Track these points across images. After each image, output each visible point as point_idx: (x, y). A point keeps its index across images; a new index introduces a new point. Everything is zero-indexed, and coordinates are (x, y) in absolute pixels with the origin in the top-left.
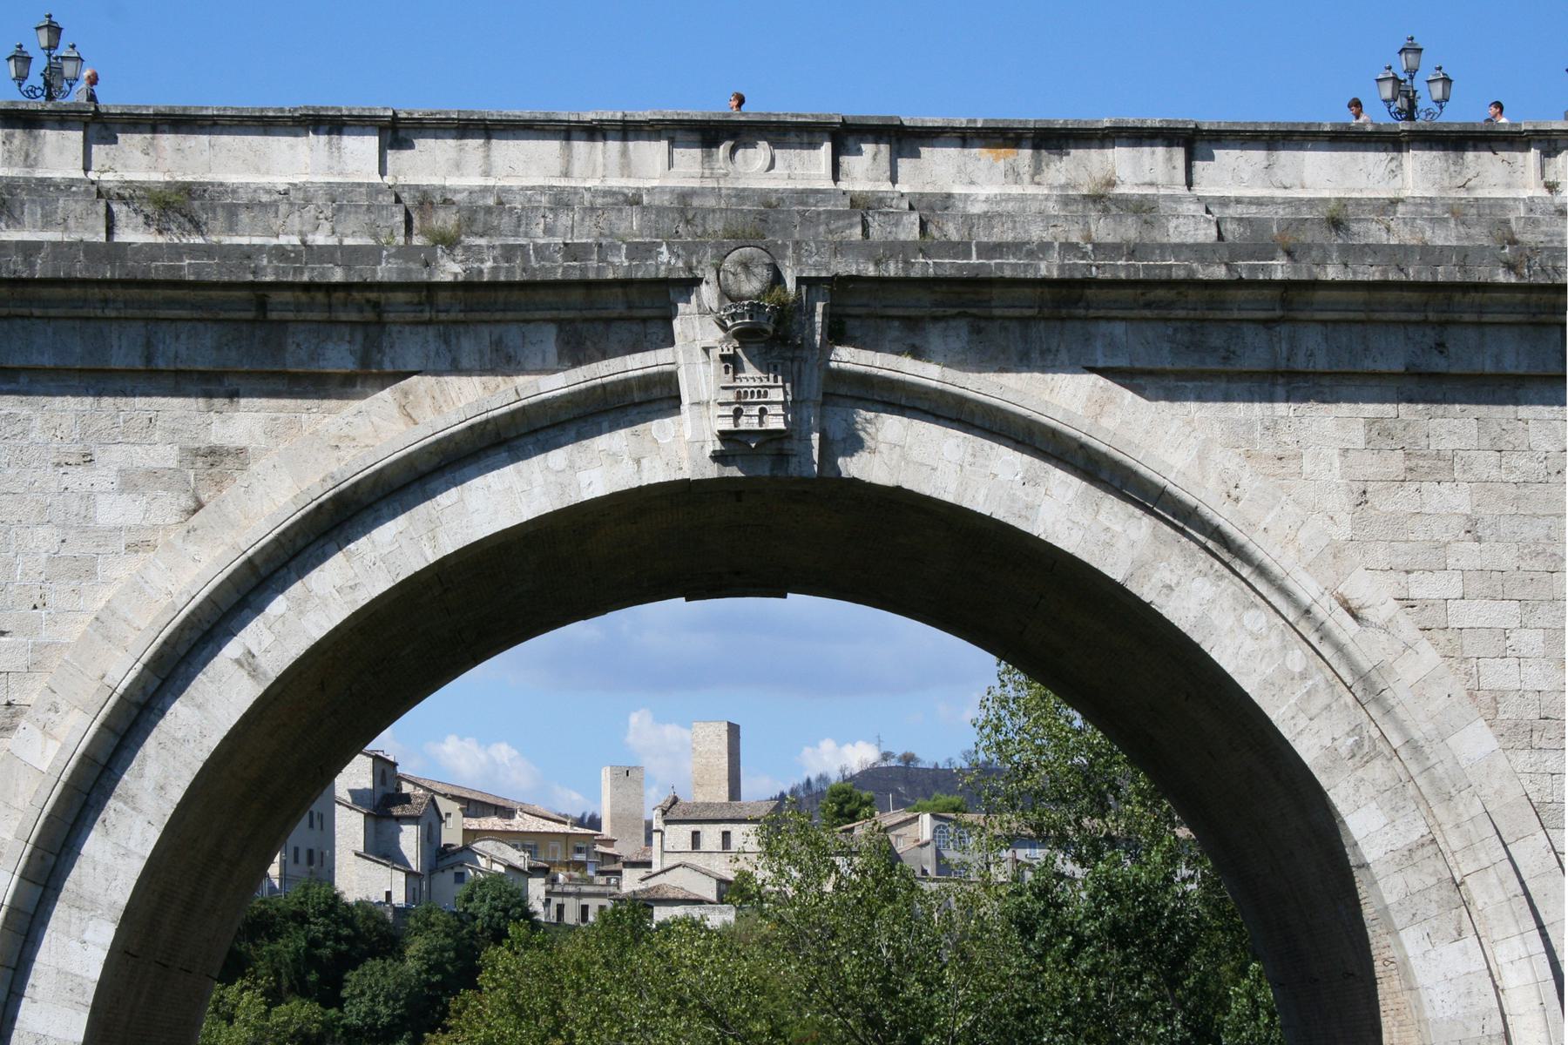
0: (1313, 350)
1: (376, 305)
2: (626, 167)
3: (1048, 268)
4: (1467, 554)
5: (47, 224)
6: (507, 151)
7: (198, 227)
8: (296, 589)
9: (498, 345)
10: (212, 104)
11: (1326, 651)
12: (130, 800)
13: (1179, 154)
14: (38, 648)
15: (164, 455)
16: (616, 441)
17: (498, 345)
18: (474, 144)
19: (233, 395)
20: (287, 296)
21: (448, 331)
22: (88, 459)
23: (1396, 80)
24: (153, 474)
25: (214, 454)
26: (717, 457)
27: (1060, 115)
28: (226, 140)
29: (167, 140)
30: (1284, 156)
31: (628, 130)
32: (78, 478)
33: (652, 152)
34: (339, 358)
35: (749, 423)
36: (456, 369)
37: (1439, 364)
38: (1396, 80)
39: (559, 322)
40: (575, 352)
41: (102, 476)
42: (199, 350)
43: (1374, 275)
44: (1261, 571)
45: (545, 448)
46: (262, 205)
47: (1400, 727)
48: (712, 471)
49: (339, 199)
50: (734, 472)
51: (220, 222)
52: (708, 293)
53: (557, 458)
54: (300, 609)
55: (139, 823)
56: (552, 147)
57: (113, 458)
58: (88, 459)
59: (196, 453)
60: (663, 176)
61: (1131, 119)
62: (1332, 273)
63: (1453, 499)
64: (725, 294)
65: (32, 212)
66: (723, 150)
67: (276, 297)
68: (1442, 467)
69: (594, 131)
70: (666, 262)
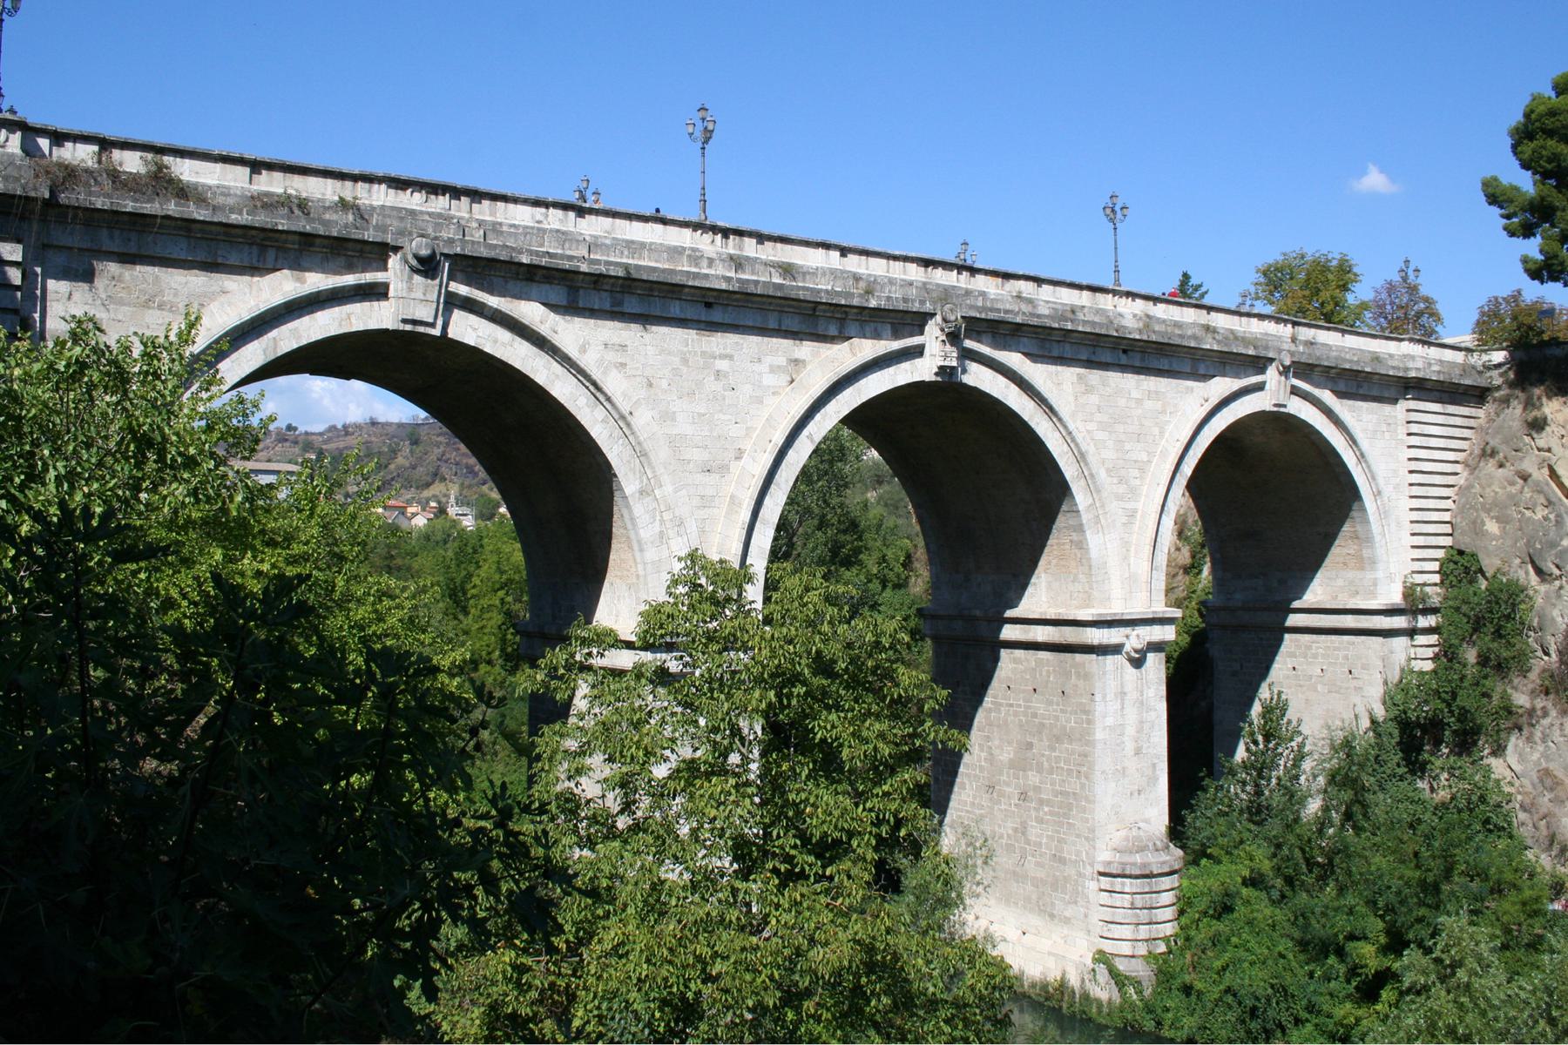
0: (1068, 351)
1: (846, 313)
2: (493, 214)
3: (1019, 320)
4: (1098, 417)
5: (753, 273)
6: (873, 261)
7: (795, 279)
8: (823, 411)
9: (876, 330)
10: (518, 193)
11: (1072, 445)
12: (778, 485)
13: (248, 170)
14: (747, 428)
15: (782, 361)
16: (906, 365)
17: (876, 330)
18: (864, 258)
19: (801, 340)
20: (824, 307)
21: (863, 323)
22: (760, 360)
23: (580, 192)
24: (779, 367)
25: (796, 362)
26: (936, 374)
27: (1010, 270)
28: (796, 248)
29: (779, 245)
30: (1058, 288)
31: (906, 259)
32: (757, 367)
33: (912, 267)
34: (833, 331)
35: (947, 363)
36: (865, 337)
37: (1094, 358)
38: (580, 192)
39: (891, 323)
40: (897, 335)
41: (764, 367)
42: (792, 323)
43: (1088, 330)
44: (1060, 420)
45: (889, 366)
46: (814, 273)
47: (1089, 469)
48: (933, 378)
49: (834, 274)
50: (939, 379)
51: (800, 278)
52: (938, 318)
53: (891, 370)
54: (824, 418)
55: (780, 493)
56: (884, 261)
57: (768, 360)
58: (760, 360)
59: (791, 361)
60: (421, 205)
61: (1027, 273)
62: (1080, 329)
63: (1094, 399)
64: (945, 320)
65: (748, 268)
66: (930, 269)
67: (821, 307)
68: (1089, 390)
69: (896, 258)
70: (928, 307)
